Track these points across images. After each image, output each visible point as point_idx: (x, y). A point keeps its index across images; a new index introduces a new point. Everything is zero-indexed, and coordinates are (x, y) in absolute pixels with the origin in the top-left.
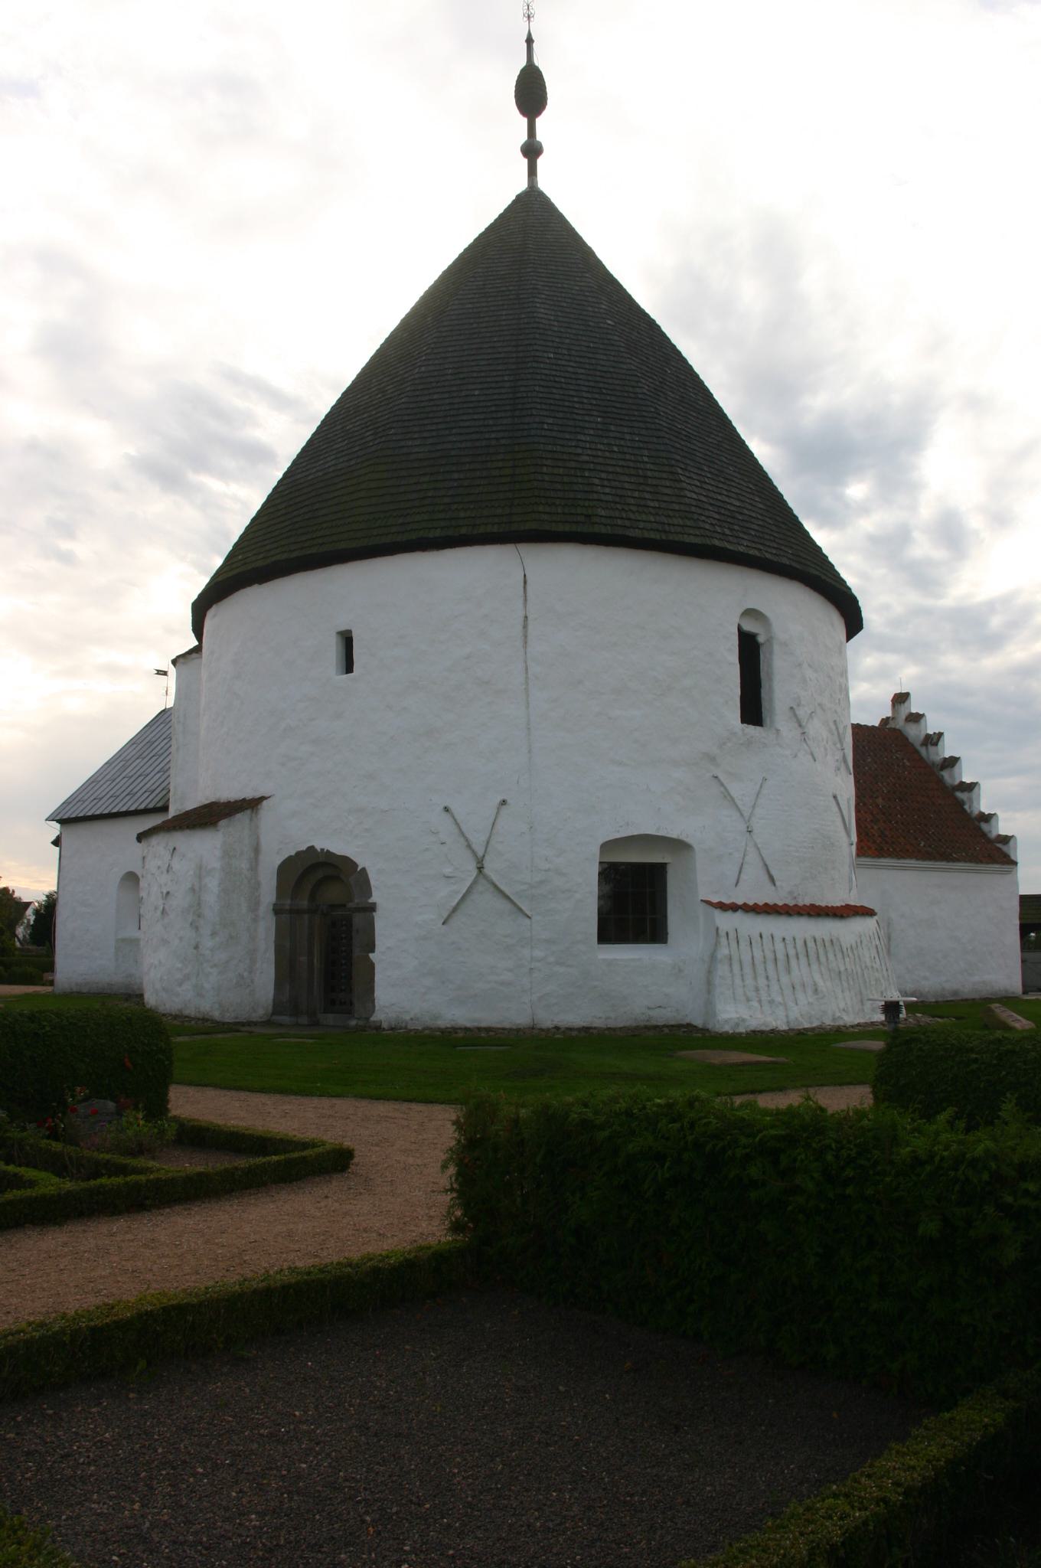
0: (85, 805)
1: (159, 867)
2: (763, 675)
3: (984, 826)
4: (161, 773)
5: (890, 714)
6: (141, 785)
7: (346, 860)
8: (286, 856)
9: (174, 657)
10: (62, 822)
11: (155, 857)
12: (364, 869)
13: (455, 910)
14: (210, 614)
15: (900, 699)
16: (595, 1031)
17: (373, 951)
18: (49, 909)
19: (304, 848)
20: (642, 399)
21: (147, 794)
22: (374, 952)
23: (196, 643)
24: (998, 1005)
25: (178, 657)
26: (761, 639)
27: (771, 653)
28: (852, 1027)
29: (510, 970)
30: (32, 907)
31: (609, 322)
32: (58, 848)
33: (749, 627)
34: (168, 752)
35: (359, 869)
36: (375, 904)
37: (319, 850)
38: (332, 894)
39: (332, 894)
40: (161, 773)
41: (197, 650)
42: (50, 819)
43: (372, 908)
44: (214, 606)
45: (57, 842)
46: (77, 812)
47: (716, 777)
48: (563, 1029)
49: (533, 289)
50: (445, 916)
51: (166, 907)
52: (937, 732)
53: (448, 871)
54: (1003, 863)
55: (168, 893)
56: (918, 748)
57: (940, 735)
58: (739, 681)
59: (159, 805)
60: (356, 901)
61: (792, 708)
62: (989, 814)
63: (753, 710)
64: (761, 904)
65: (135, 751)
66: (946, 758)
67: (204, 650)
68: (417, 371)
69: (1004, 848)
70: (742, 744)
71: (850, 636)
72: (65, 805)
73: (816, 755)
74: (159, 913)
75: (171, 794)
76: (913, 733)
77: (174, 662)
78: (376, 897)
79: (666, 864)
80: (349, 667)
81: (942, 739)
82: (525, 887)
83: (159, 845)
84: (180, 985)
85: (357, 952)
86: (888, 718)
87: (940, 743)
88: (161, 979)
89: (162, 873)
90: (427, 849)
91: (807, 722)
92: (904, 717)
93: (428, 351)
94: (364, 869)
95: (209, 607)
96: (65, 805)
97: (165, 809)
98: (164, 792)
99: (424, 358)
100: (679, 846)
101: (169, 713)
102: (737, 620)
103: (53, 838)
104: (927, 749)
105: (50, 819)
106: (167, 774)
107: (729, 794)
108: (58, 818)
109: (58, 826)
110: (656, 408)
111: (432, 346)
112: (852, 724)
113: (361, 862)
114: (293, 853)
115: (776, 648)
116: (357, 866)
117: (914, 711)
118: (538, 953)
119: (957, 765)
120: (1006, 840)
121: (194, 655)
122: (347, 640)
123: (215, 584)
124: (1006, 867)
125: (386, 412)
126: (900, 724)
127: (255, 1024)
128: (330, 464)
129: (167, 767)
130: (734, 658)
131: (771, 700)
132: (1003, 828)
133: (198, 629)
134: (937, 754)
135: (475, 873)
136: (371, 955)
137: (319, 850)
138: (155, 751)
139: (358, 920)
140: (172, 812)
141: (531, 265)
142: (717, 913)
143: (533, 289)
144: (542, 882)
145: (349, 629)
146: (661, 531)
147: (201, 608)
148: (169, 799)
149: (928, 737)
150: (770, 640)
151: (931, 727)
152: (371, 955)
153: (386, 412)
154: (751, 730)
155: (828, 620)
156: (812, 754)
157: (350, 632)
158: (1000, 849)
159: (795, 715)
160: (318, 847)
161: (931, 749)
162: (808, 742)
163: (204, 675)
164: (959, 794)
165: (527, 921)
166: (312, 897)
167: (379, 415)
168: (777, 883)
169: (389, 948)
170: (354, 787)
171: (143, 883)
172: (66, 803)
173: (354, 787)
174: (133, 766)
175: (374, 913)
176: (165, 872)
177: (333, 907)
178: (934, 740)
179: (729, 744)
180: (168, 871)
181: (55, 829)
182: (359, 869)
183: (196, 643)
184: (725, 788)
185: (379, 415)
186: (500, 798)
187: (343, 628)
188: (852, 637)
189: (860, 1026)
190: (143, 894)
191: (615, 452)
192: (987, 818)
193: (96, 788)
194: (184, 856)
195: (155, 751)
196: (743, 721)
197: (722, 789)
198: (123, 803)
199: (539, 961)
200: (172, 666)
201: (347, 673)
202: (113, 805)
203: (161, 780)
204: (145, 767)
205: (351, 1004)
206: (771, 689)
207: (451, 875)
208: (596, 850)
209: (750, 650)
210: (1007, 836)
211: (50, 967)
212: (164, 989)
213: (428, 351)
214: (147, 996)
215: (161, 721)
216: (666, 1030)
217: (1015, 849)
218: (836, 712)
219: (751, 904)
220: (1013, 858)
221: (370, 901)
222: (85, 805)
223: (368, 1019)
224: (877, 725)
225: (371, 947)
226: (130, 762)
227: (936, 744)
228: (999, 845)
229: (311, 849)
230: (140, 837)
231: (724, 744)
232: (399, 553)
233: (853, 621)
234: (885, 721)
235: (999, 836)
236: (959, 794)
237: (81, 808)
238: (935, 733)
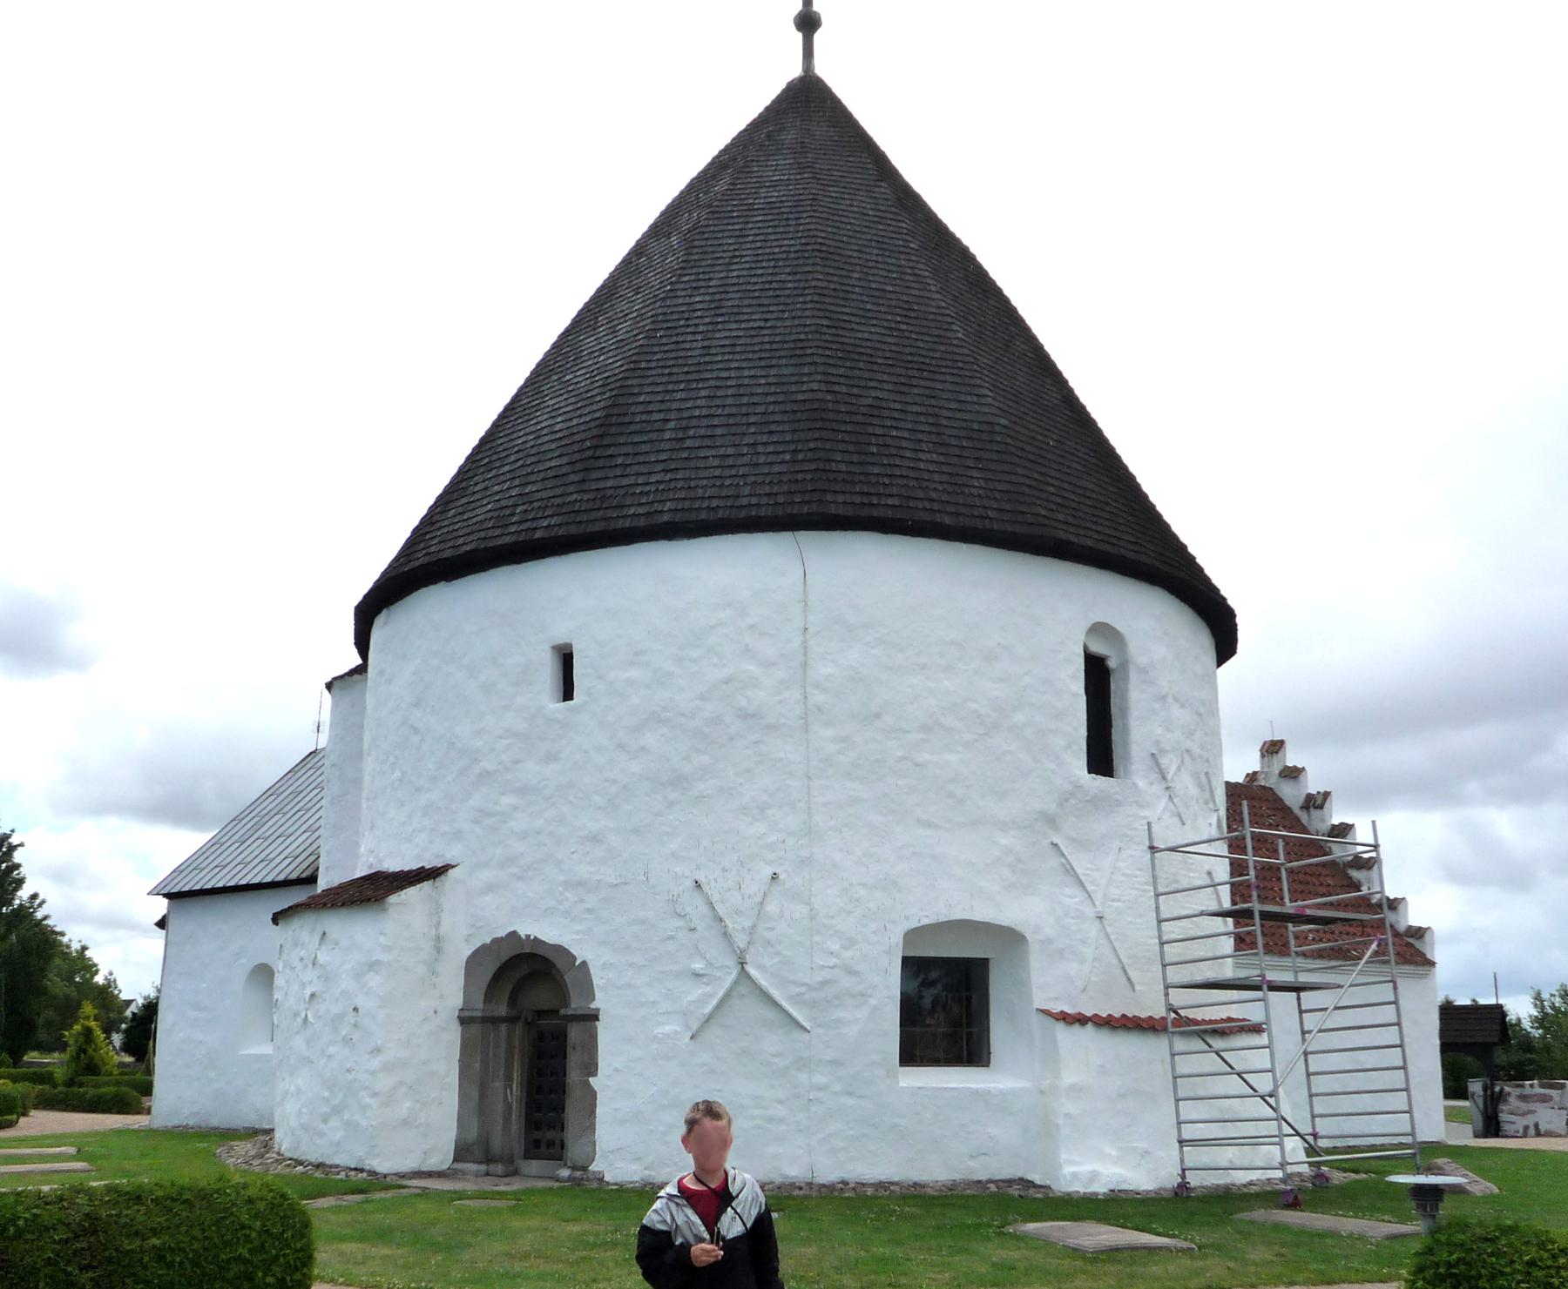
0: (201, 875)
1: (302, 959)
2: (1114, 711)
3: (1390, 917)
4: (309, 834)
5: (1257, 769)
6: (280, 849)
7: (560, 949)
8: (479, 944)
9: (330, 679)
10: (168, 896)
11: (297, 946)
12: (584, 963)
13: (708, 1020)
14: (379, 622)
15: (1273, 748)
16: (896, 1188)
17: (594, 1074)
18: (151, 1009)
19: (502, 933)
20: (956, 346)
21: (282, 839)
22: (596, 1075)
23: (359, 661)
24: (1446, 1160)
25: (335, 679)
26: (1112, 664)
27: (1126, 680)
28: (1245, 1186)
29: (780, 1102)
30: (134, 1004)
31: (912, 245)
32: (164, 932)
33: (1097, 648)
34: (318, 806)
35: (577, 964)
36: (598, 1010)
37: (524, 937)
38: (539, 997)
39: (539, 997)
40: (309, 834)
41: (361, 670)
42: (154, 892)
43: (594, 1017)
44: (384, 612)
45: (161, 924)
46: (192, 883)
47: (1056, 845)
48: (852, 1185)
49: (813, 199)
50: (695, 1027)
51: (317, 946)
52: (1322, 791)
53: (698, 966)
54: (1416, 963)
55: (313, 995)
56: (1297, 811)
57: (1327, 795)
58: (1085, 717)
59: (304, 875)
60: (573, 1006)
61: (1153, 755)
62: (1396, 899)
63: (1101, 758)
64: (1117, 1015)
65: (274, 804)
66: (1334, 826)
67: (370, 669)
68: (658, 304)
69: (1417, 944)
70: (1087, 801)
71: (1220, 661)
72: (174, 875)
73: (1184, 817)
74: (299, 1020)
75: (321, 860)
76: (1291, 795)
77: (329, 686)
78: (600, 1002)
79: (987, 959)
80: (568, 694)
81: (1328, 801)
82: (803, 989)
83: (303, 930)
84: (325, 1121)
85: (573, 1076)
86: (1255, 773)
87: (1326, 806)
88: (300, 1111)
89: (306, 966)
90: (670, 938)
91: (1175, 774)
92: (1277, 772)
93: (673, 279)
94: (584, 963)
95: (378, 612)
96: (174, 875)
97: (312, 880)
98: (312, 858)
99: (669, 288)
100: (1011, 938)
101: (321, 755)
102: (1080, 637)
103: (159, 917)
104: (1309, 815)
105: (154, 892)
106: (317, 834)
107: (1073, 869)
108: (165, 891)
109: (165, 901)
110: (975, 358)
111: (678, 272)
112: (1227, 783)
113: (581, 953)
114: (488, 941)
115: (1133, 676)
116: (574, 958)
117: (1290, 764)
118: (819, 1079)
119: (1351, 832)
120: (1419, 933)
121: (356, 677)
122: (566, 659)
123: (389, 579)
124: (1421, 970)
125: (618, 358)
126: (1272, 781)
127: (430, 1175)
128: (543, 425)
129: (318, 824)
130: (1078, 686)
131: (1126, 744)
132: (1415, 916)
133: (362, 642)
134: (1323, 820)
135: (735, 973)
136: (591, 1079)
137: (524, 937)
138: (301, 805)
139: (575, 1033)
140: (323, 884)
141: (809, 170)
142: (1060, 1028)
143: (813, 199)
144: (825, 983)
145: (568, 641)
146: (986, 518)
147: (368, 613)
148: (318, 868)
149: (1310, 797)
150: (1124, 665)
151: (1313, 784)
152: (591, 1079)
153: (618, 358)
154: (1101, 781)
155: (1195, 638)
156: (1180, 817)
157: (570, 646)
158: (1412, 945)
159: (1158, 764)
160: (523, 934)
161: (1315, 813)
162: (1175, 800)
163: (370, 701)
164: (1355, 874)
165: (807, 1034)
166: (513, 1001)
167: (610, 361)
168: (1138, 988)
169: (617, 1070)
170: (573, 853)
171: (279, 980)
172: (178, 871)
173: (573, 853)
174: (270, 823)
175: (597, 1023)
176: (311, 965)
177: (540, 1013)
178: (1315, 802)
179: (1073, 801)
180: (314, 964)
181: (161, 906)
182: (577, 964)
183: (359, 661)
184: (1067, 860)
185: (610, 361)
186: (769, 871)
187: (560, 641)
188: (1224, 662)
189: (1254, 1185)
190: (277, 995)
191: (873, 454)
192: (1394, 904)
193: (219, 852)
194: (337, 944)
195: (301, 805)
196: (1089, 772)
197: (1063, 860)
198: (255, 871)
199: (820, 1089)
200: (326, 691)
201: (564, 701)
202: (241, 875)
203: (310, 841)
204: (287, 825)
205: (563, 1146)
206: (1126, 731)
207: (701, 972)
208: (897, 938)
209: (1098, 675)
210: (1420, 928)
211: (147, 1089)
212: (302, 1126)
213: (673, 279)
214: (278, 1135)
215: (308, 766)
216: (993, 1187)
217: (1432, 944)
218: (1208, 761)
219: (1104, 1016)
220: (1429, 956)
221: (593, 1006)
222: (201, 875)
223: (585, 1169)
224: (1241, 782)
225: (591, 1068)
226: (267, 817)
227: (1321, 807)
228: (1410, 940)
229: (513, 935)
230: (276, 919)
231: (1066, 800)
232: (637, 542)
233: (1224, 640)
234: (1252, 777)
235: (1410, 927)
236: (1355, 874)
237: (197, 879)
238: (1319, 793)
